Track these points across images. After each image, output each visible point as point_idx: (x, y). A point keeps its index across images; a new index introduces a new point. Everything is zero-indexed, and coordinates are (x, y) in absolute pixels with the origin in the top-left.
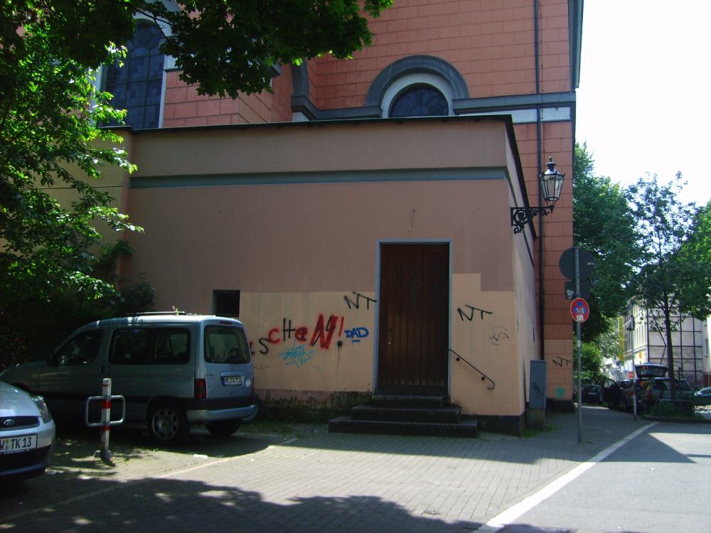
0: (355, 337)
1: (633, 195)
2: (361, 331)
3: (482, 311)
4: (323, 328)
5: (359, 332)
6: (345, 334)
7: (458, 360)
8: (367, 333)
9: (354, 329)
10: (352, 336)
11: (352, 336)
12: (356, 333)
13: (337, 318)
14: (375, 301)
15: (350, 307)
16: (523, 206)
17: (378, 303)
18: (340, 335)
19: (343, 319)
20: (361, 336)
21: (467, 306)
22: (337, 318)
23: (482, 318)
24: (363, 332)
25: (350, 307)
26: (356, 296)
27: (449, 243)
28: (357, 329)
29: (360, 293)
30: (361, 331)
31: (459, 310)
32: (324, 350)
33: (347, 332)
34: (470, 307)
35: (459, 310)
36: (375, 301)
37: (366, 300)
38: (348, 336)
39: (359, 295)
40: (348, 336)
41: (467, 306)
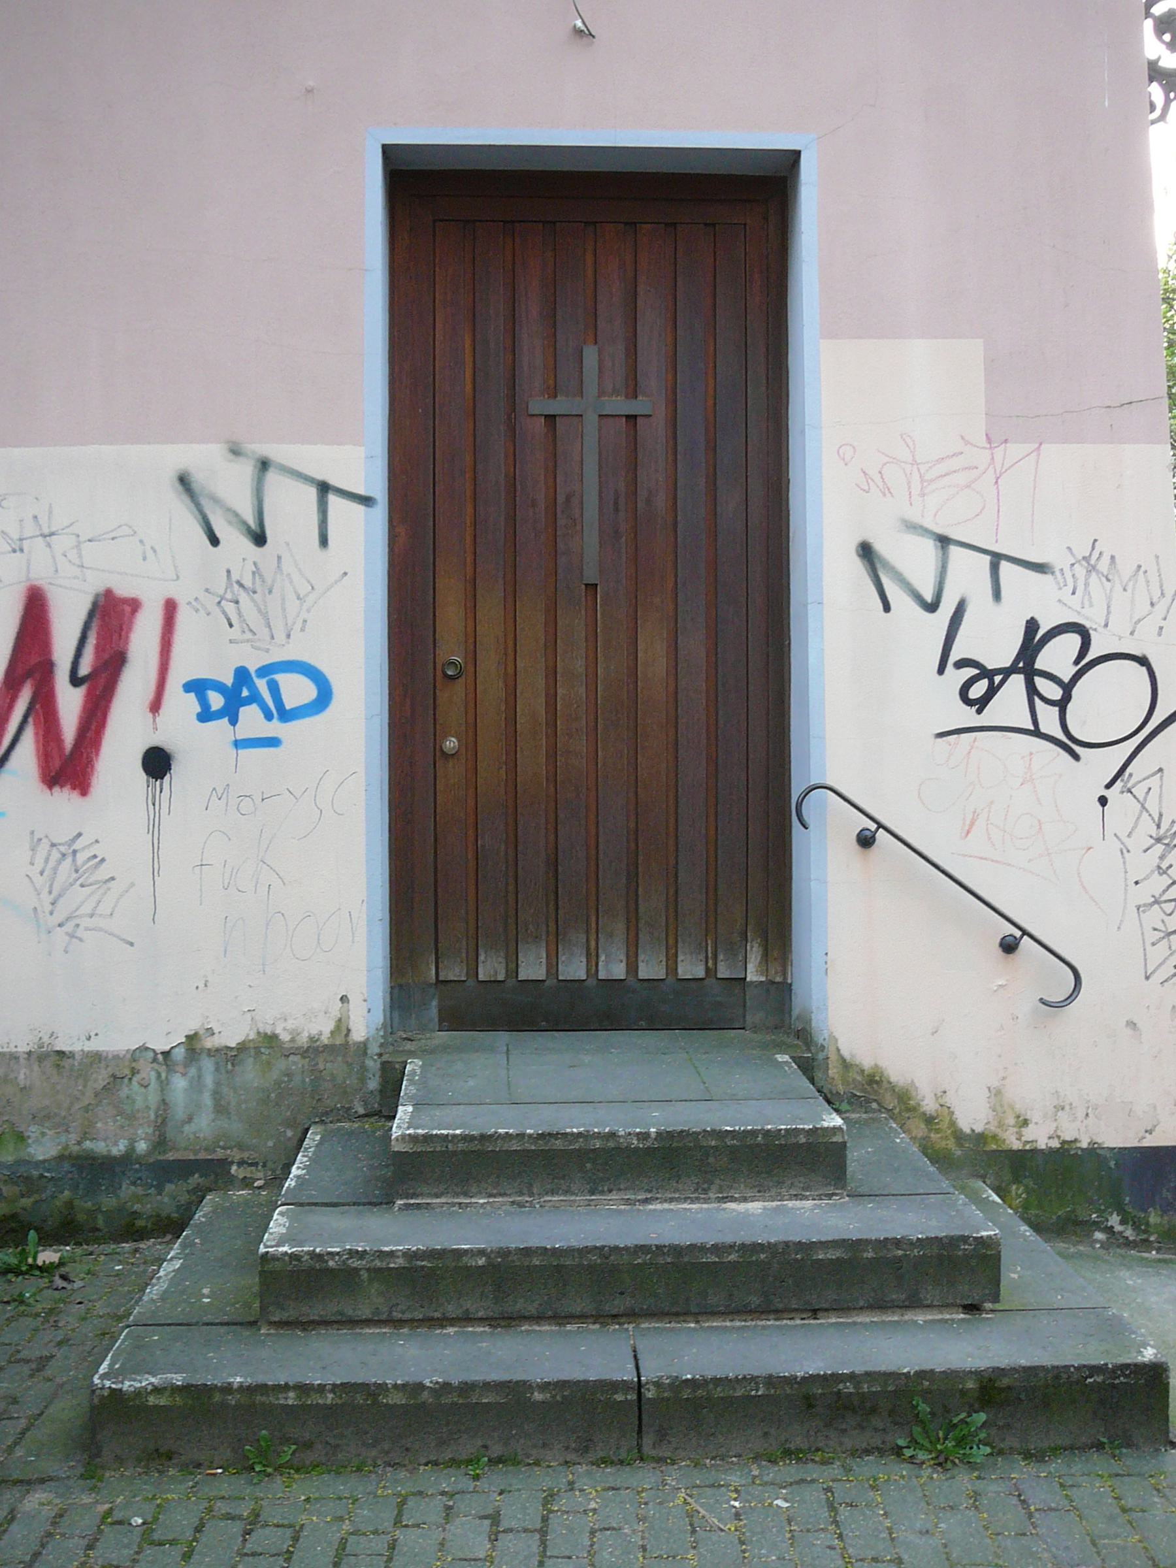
0: (251, 720)
1: (17, 549)
2: (281, 678)
3: (996, 558)
4: (46, 669)
5: (274, 688)
6: (191, 703)
7: (866, 841)
8: (324, 697)
9: (242, 675)
10: (231, 713)
11: (231, 713)
12: (255, 698)
13: (134, 605)
14: (366, 501)
15: (214, 541)
16: (522, 976)
17: (379, 514)
18: (156, 706)
19: (170, 608)
20: (286, 715)
21: (914, 528)
22: (134, 605)
23: (997, 595)
24: (295, 690)
25: (214, 541)
26: (246, 470)
27: (794, 157)
28: (264, 671)
29: (276, 451)
30: (281, 678)
31: (866, 551)
32: (64, 799)
33: (197, 687)
34: (926, 532)
35: (866, 551)
36: (366, 501)
37: (312, 492)
38: (206, 715)
39: (264, 465)
40: (206, 715)
41: (914, 528)
